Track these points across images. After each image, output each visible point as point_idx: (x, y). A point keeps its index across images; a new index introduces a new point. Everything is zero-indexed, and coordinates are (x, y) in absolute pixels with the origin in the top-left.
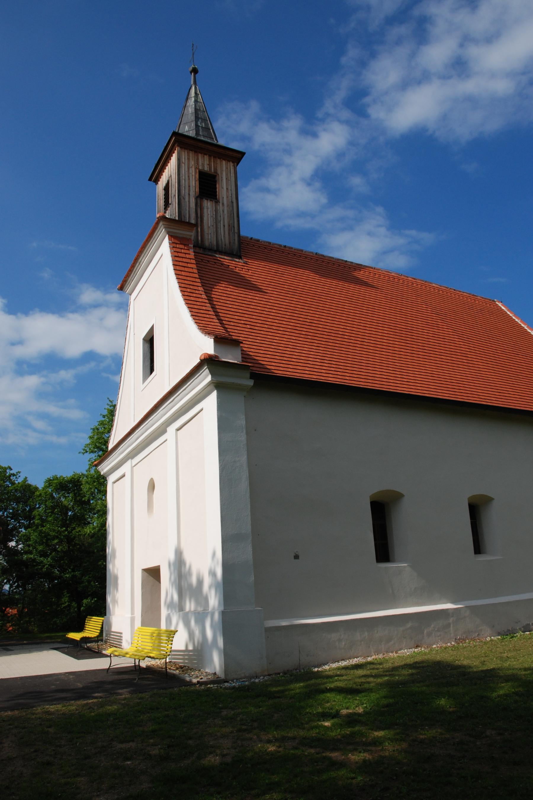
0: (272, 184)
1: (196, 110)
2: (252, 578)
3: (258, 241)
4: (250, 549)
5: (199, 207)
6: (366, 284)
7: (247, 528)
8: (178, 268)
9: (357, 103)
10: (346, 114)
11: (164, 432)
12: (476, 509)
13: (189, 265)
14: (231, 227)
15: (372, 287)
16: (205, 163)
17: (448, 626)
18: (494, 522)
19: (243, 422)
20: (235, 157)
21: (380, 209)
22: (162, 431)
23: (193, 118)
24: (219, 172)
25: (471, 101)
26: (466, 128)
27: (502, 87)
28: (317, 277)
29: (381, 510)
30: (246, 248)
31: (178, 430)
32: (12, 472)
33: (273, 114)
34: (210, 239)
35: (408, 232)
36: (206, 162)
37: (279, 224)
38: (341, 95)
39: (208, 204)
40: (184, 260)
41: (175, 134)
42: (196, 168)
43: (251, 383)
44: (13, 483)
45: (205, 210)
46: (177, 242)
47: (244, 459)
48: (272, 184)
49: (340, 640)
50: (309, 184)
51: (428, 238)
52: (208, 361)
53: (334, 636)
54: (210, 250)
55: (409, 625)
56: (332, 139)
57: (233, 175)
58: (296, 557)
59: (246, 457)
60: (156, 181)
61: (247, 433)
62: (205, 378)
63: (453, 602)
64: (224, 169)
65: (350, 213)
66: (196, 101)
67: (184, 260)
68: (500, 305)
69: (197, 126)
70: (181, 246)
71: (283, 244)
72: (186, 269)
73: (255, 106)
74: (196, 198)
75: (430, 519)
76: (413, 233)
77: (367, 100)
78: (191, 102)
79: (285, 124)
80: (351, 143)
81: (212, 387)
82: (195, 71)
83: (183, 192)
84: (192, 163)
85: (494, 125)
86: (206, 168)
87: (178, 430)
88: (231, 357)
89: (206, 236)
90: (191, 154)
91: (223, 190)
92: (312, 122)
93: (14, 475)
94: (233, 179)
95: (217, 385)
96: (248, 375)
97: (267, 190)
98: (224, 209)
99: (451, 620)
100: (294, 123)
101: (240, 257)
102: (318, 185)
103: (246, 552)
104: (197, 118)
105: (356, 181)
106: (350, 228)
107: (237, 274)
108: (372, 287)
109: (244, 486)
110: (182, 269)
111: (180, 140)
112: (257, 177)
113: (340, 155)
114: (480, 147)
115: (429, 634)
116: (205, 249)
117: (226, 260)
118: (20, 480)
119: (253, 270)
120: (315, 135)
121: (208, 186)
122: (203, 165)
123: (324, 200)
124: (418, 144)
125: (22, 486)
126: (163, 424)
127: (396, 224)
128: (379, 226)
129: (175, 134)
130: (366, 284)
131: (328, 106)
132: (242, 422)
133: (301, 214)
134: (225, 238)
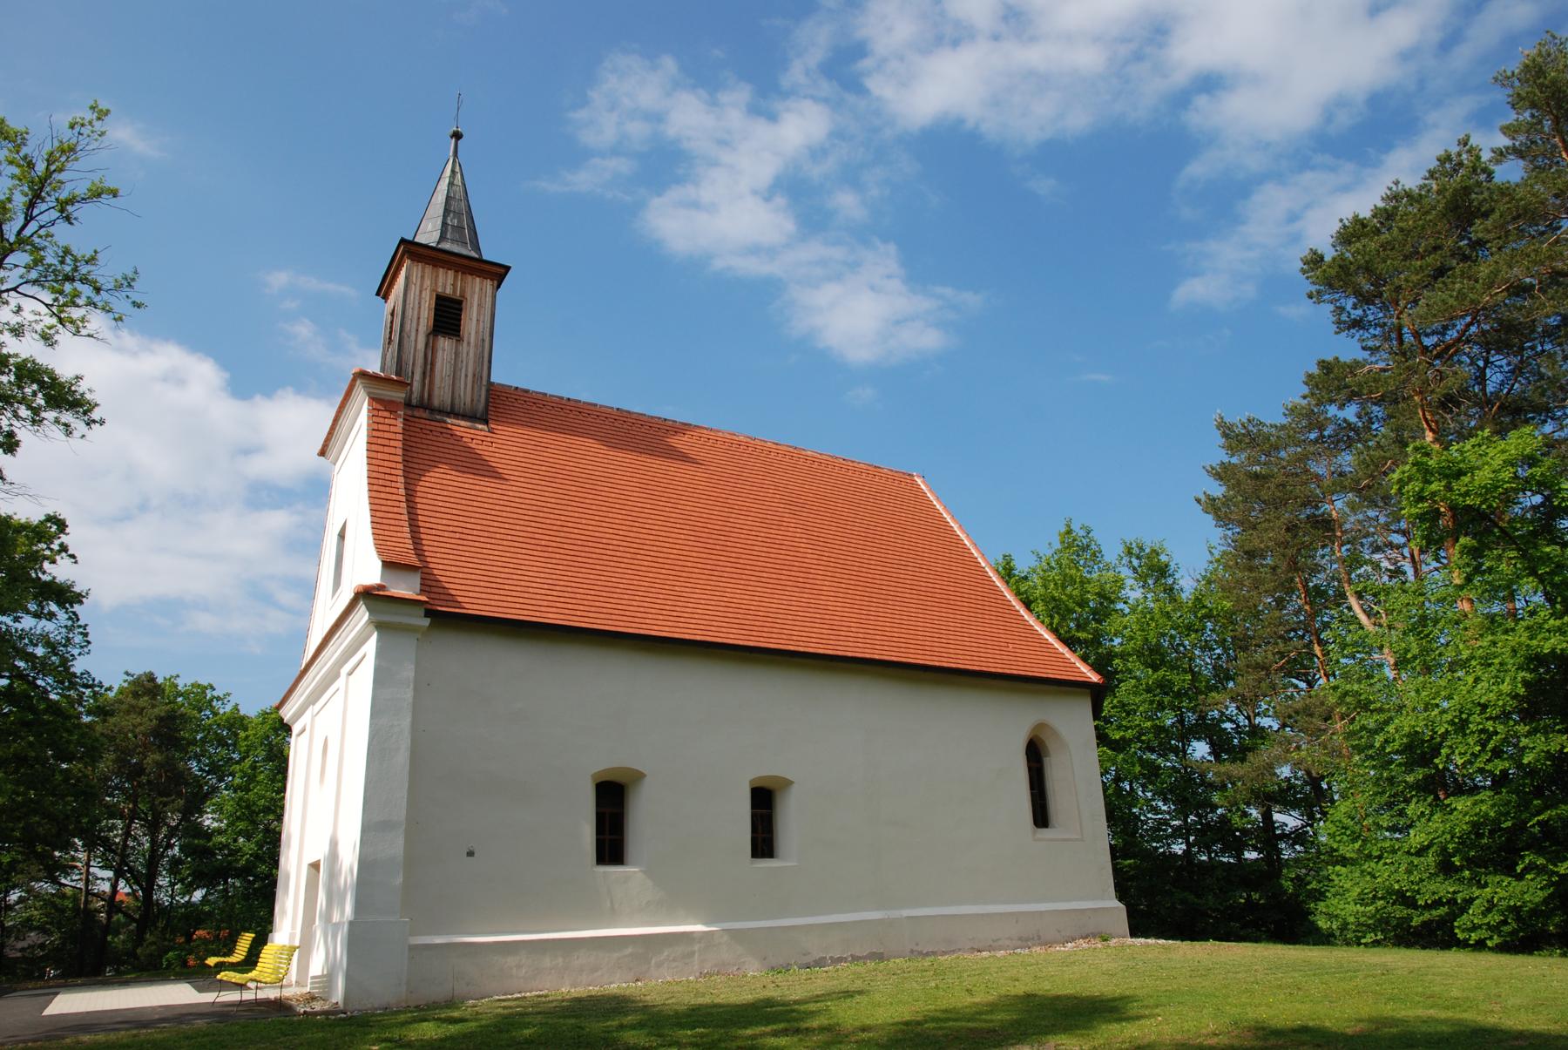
0: (706, 194)
1: (448, 198)
2: (399, 880)
3: (527, 391)
4: (401, 841)
5: (430, 348)
6: (685, 458)
7: (400, 813)
8: (374, 447)
9: (845, 68)
10: (827, 88)
11: (337, 676)
12: (764, 800)
13: (392, 443)
14: (477, 377)
15: (694, 461)
16: (447, 282)
17: (693, 953)
18: (791, 820)
19: (412, 674)
20: (497, 273)
21: (892, 248)
22: (333, 676)
23: (441, 212)
24: (468, 296)
25: (1041, 81)
26: (1035, 120)
27: (1088, 59)
28: (603, 450)
29: (612, 798)
30: (498, 404)
31: (350, 674)
32: (215, 694)
33: (702, 78)
34: (441, 396)
35: (939, 290)
36: (450, 281)
37: (718, 264)
38: (816, 56)
39: (445, 344)
40: (387, 435)
41: (403, 241)
42: (432, 291)
43: (426, 622)
44: (215, 714)
45: (440, 354)
46: (381, 405)
47: (406, 722)
48: (706, 194)
49: (519, 967)
50: (767, 200)
51: (972, 300)
52: (366, 595)
53: (511, 961)
54: (441, 412)
55: (629, 950)
56: (801, 127)
57: (489, 299)
58: (470, 854)
59: (409, 720)
60: (386, 297)
61: (415, 689)
62: (362, 615)
63: (705, 924)
64: (476, 290)
65: (837, 253)
66: (451, 184)
67: (387, 435)
68: (919, 481)
69: (444, 224)
70: (387, 414)
71: (566, 396)
72: (386, 449)
73: (669, 64)
74: (428, 336)
75: (692, 809)
76: (948, 291)
77: (866, 64)
78: (443, 186)
79: (724, 97)
80: (838, 135)
81: (372, 627)
82: (457, 136)
83: (407, 327)
84: (428, 282)
85: (1079, 121)
86: (449, 291)
87: (350, 674)
88: (406, 588)
89: (436, 392)
90: (429, 269)
91: (471, 323)
92: (768, 97)
93: (218, 699)
94: (489, 305)
95: (380, 626)
96: (422, 612)
97: (695, 205)
98: (469, 350)
99: (696, 947)
100: (737, 96)
101: (486, 422)
102: (780, 201)
103: (395, 846)
104: (447, 211)
105: (847, 203)
106: (838, 278)
107: (471, 451)
108: (694, 461)
109: (402, 758)
110: (381, 449)
111: (410, 250)
112: (679, 181)
113: (817, 153)
114: (1055, 154)
115: (659, 965)
116: (432, 410)
117: (460, 427)
118: (228, 708)
119: (501, 443)
120: (772, 118)
121: (447, 316)
122: (445, 287)
123: (790, 226)
124: (952, 149)
125: (228, 720)
126: (335, 664)
127: (918, 274)
128: (889, 277)
129: (403, 241)
130: (685, 458)
131: (796, 74)
132: (408, 672)
133: (755, 250)
134: (467, 394)
